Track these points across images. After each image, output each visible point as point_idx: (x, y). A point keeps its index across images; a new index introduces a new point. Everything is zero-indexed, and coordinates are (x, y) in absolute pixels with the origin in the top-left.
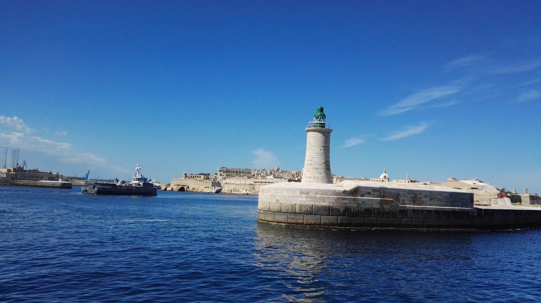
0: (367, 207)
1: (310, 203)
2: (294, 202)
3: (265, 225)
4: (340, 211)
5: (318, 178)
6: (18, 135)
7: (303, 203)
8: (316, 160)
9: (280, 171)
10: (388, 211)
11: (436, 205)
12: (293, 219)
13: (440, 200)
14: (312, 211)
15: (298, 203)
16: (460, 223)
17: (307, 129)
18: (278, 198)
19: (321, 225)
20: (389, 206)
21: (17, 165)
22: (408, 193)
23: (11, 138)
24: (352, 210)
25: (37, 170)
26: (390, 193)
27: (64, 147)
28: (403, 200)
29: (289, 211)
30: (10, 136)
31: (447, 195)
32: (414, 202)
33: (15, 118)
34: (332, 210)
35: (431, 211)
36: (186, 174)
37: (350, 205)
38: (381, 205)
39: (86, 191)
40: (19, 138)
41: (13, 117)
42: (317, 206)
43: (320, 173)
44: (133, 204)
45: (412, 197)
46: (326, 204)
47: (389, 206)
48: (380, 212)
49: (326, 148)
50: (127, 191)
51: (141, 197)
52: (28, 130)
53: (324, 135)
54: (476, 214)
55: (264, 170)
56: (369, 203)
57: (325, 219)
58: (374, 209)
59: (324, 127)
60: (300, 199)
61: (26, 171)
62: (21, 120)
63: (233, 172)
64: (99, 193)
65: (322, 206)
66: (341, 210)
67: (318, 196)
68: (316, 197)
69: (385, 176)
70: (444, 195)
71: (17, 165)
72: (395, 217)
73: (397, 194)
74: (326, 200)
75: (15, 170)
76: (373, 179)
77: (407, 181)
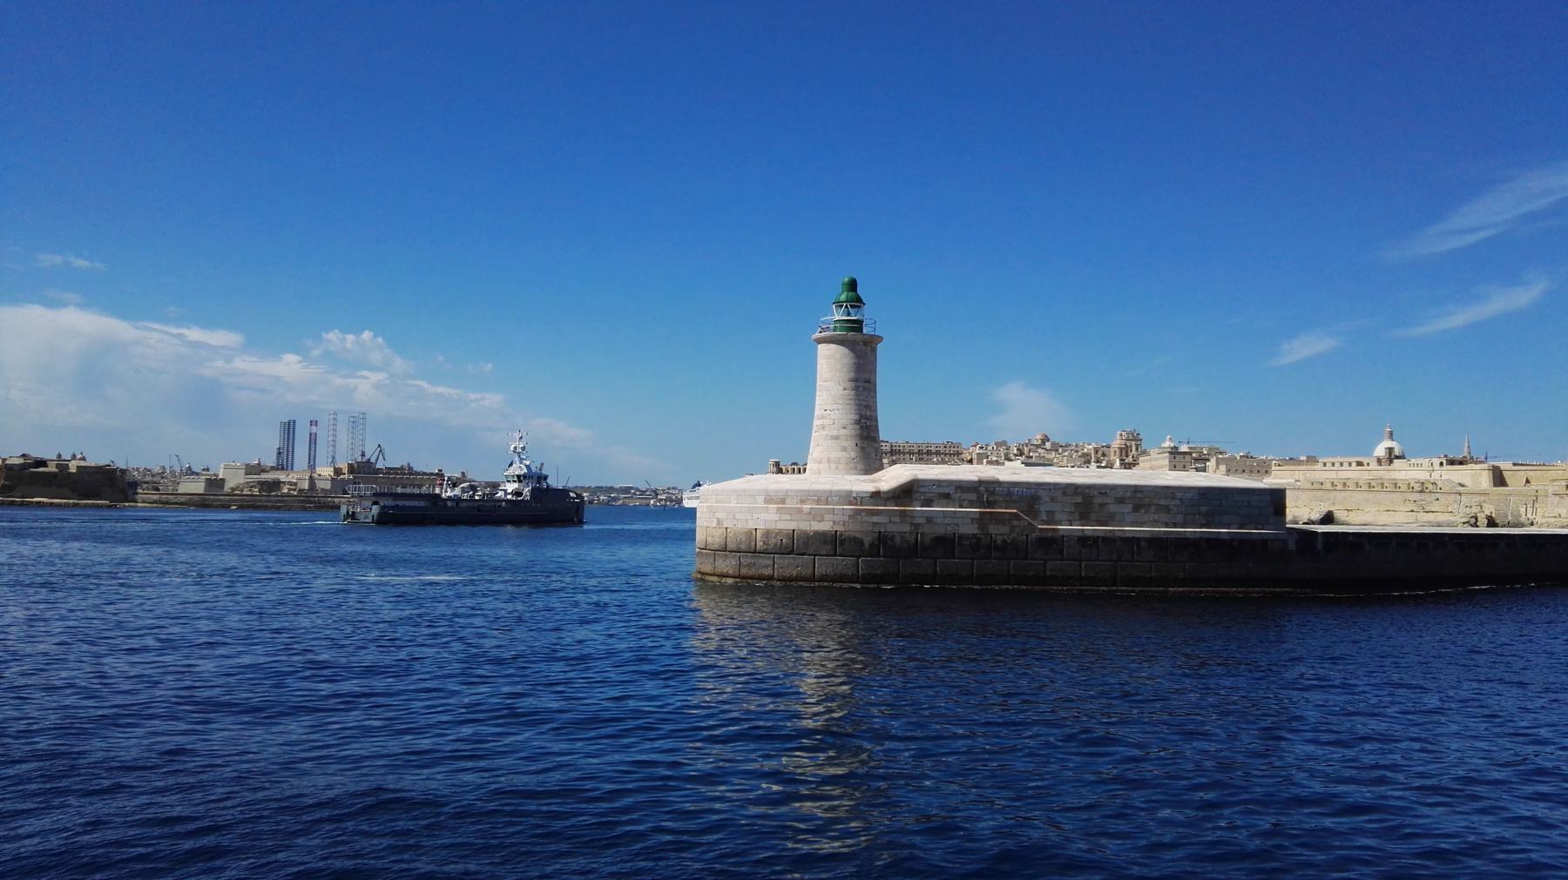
0: (940, 531)
1: (787, 524)
2: (751, 526)
3: (702, 580)
4: (862, 543)
5: (838, 461)
6: (375, 377)
7: (772, 526)
8: (836, 415)
9: (1048, 445)
10: (1004, 541)
11: (1155, 523)
12: (749, 566)
13: (1167, 509)
14: (794, 545)
15: (761, 526)
16: (1240, 570)
17: (817, 335)
18: (720, 515)
19: (813, 580)
20: (1006, 529)
21: (363, 455)
22: (1065, 494)
23: (356, 388)
24: (898, 540)
25: (410, 469)
26: (1009, 494)
27: (486, 403)
28: (1050, 513)
29: (743, 547)
30: (352, 382)
31: (1189, 495)
32: (1084, 518)
33: (367, 335)
34: (842, 542)
35: (1139, 539)
36: (777, 464)
37: (890, 528)
38: (982, 526)
39: (353, 516)
40: (378, 386)
41: (362, 332)
42: (805, 532)
43: (844, 449)
44: (505, 548)
45: (1077, 504)
46: (825, 526)
47: (1006, 529)
48: (979, 546)
49: (863, 384)
50: (481, 513)
51: (524, 530)
52: (399, 364)
53: (852, 350)
54: (1292, 546)
55: (1004, 443)
56: (947, 521)
57: (823, 566)
58: (961, 537)
59: (860, 330)
60: (763, 516)
61: (379, 471)
62: (380, 340)
63: (910, 453)
64: (384, 520)
65: (816, 533)
66: (867, 541)
67: (807, 507)
68: (800, 511)
69: (1390, 450)
70: (1179, 495)
71: (363, 455)
72: (1026, 558)
73: (1029, 496)
74: (827, 517)
75: (351, 469)
76: (1329, 460)
77: (1436, 461)
